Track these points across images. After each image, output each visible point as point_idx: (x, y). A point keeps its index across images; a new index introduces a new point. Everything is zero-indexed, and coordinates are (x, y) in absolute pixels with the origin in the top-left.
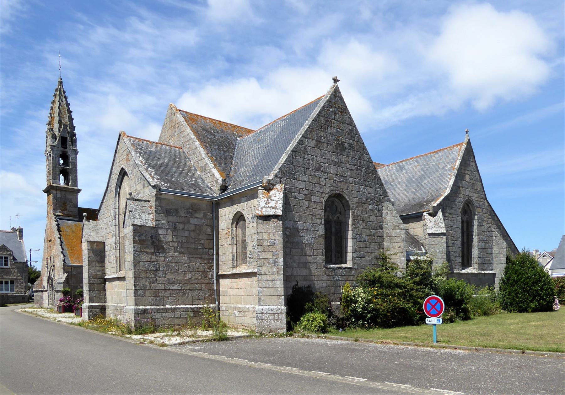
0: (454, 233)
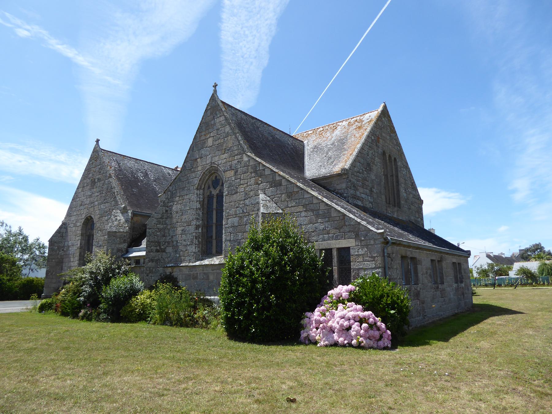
0: (184, 217)
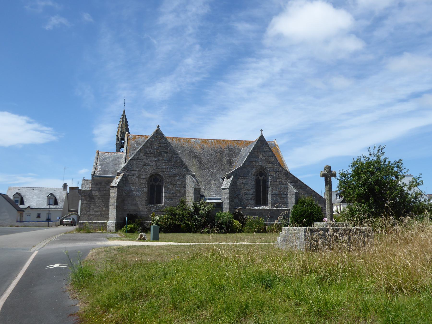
0: (246, 187)
